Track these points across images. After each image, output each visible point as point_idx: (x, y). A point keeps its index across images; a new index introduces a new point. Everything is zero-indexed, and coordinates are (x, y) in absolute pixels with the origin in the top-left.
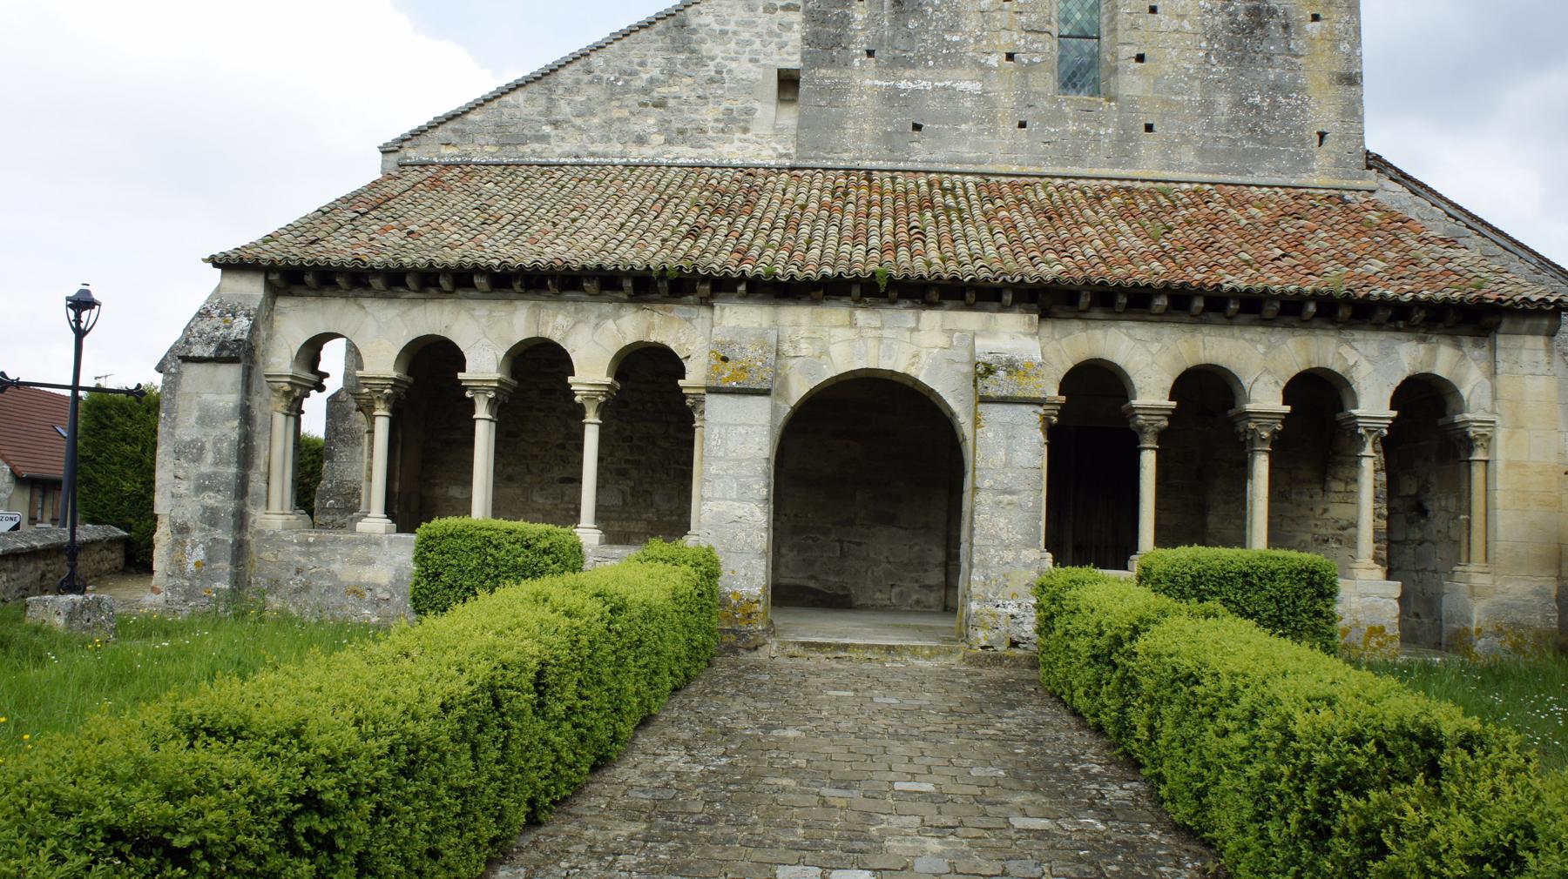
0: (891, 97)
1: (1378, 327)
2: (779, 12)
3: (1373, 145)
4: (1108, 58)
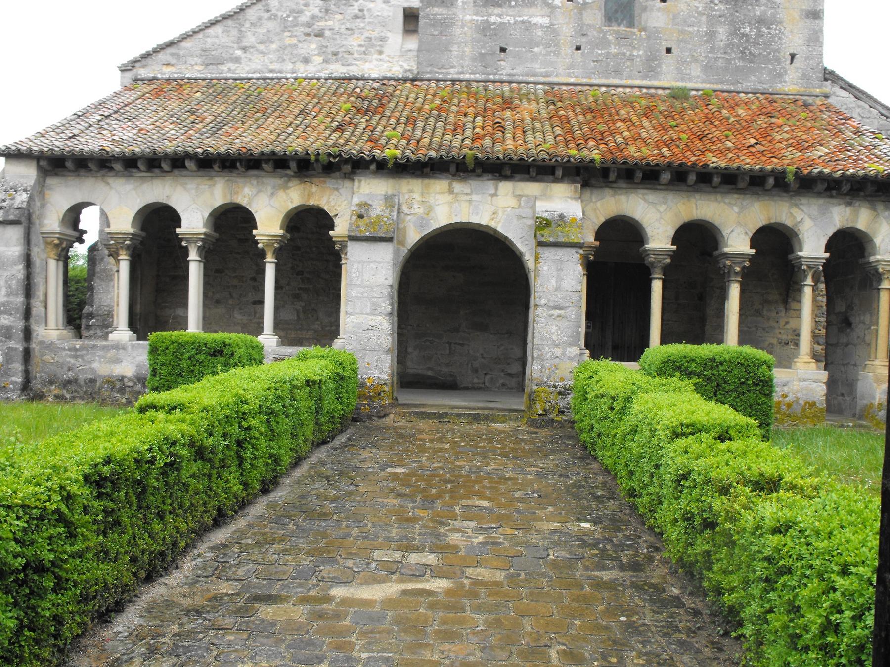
0: (485, 29)
1: (819, 195)
3: (829, 63)
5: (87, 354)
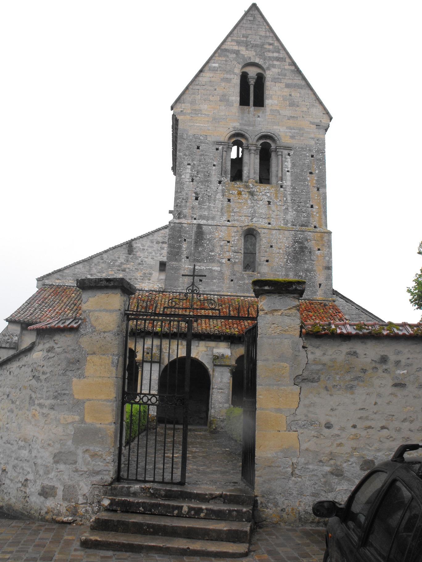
3: (335, 287)
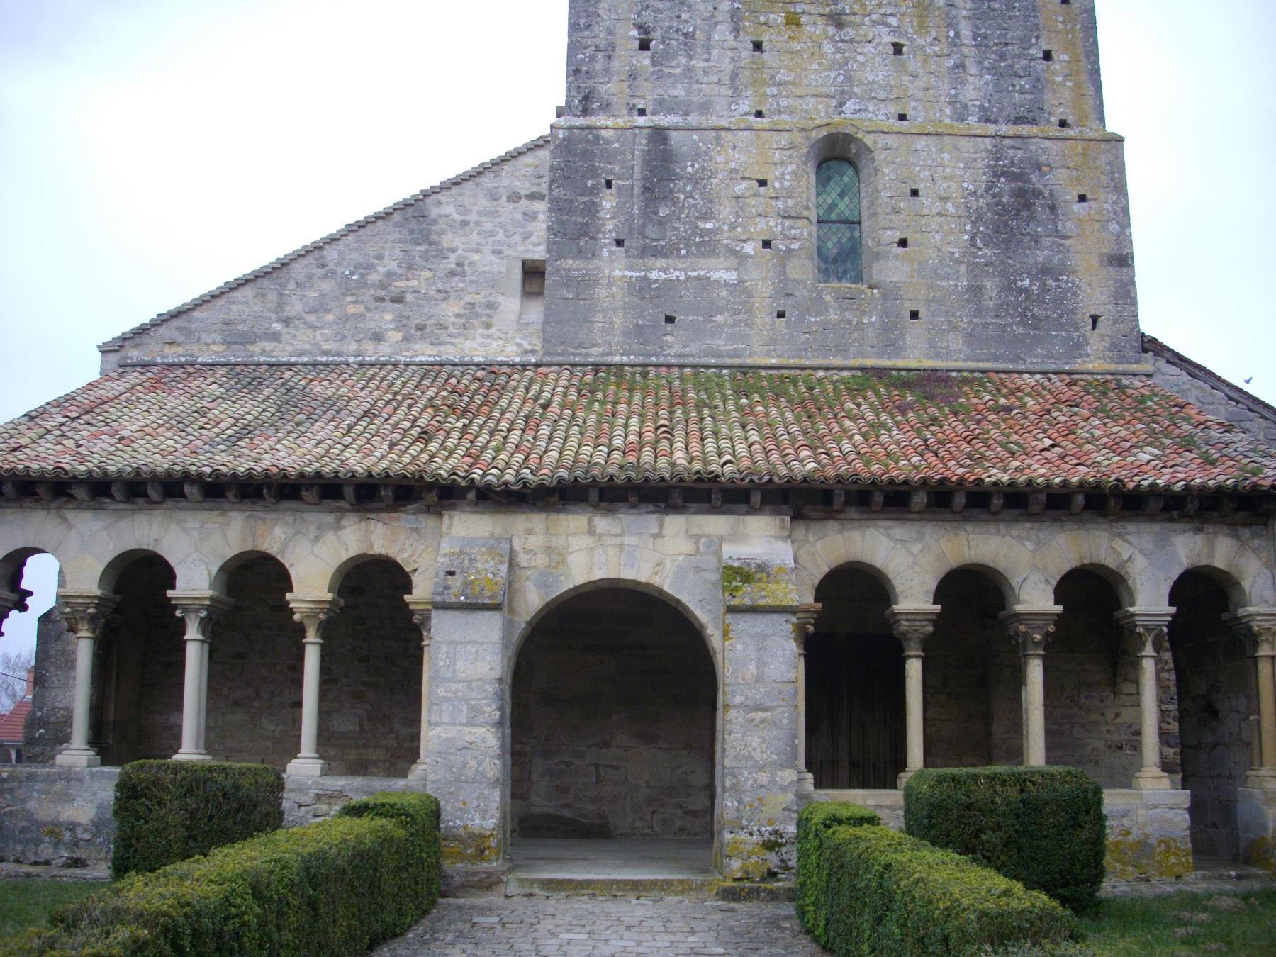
0: (642, 288)
1: (1152, 518)
2: (524, 202)
3: (1149, 326)
4: (870, 243)
5: (20, 787)
